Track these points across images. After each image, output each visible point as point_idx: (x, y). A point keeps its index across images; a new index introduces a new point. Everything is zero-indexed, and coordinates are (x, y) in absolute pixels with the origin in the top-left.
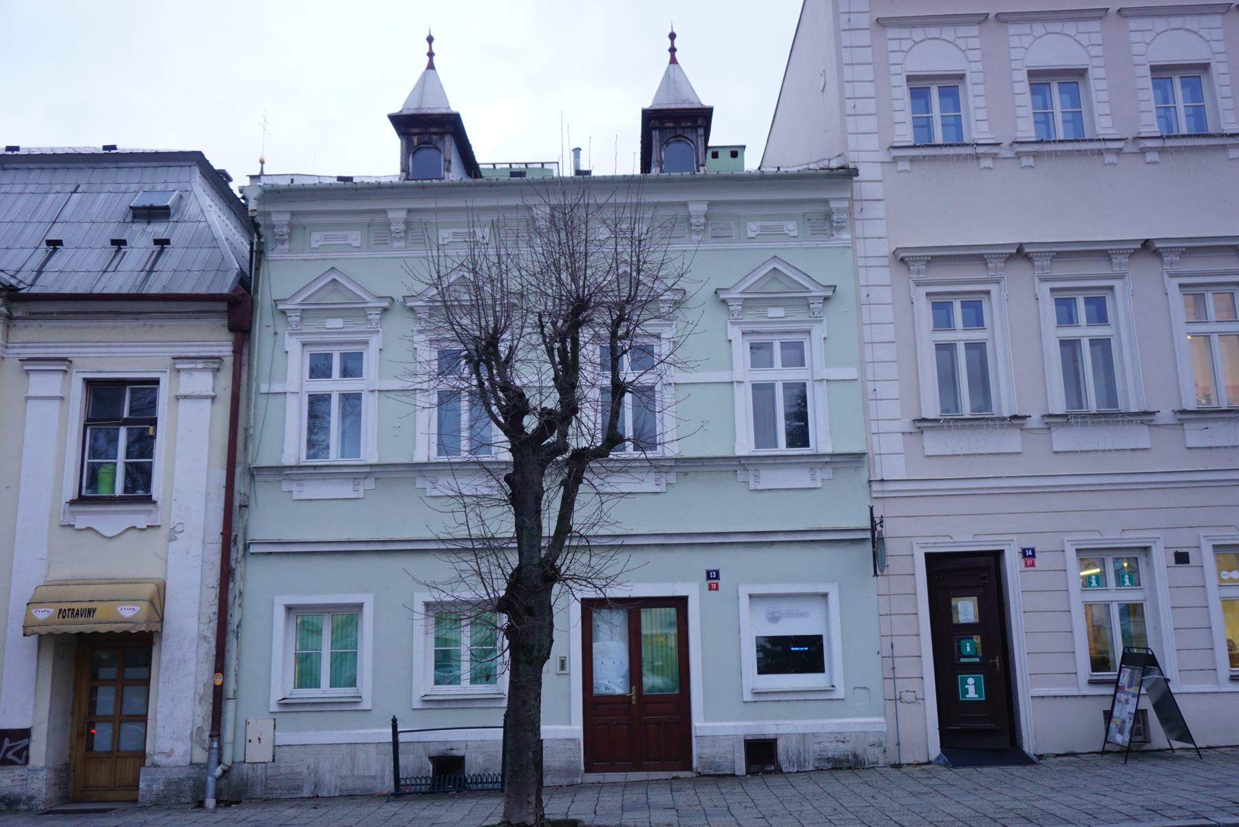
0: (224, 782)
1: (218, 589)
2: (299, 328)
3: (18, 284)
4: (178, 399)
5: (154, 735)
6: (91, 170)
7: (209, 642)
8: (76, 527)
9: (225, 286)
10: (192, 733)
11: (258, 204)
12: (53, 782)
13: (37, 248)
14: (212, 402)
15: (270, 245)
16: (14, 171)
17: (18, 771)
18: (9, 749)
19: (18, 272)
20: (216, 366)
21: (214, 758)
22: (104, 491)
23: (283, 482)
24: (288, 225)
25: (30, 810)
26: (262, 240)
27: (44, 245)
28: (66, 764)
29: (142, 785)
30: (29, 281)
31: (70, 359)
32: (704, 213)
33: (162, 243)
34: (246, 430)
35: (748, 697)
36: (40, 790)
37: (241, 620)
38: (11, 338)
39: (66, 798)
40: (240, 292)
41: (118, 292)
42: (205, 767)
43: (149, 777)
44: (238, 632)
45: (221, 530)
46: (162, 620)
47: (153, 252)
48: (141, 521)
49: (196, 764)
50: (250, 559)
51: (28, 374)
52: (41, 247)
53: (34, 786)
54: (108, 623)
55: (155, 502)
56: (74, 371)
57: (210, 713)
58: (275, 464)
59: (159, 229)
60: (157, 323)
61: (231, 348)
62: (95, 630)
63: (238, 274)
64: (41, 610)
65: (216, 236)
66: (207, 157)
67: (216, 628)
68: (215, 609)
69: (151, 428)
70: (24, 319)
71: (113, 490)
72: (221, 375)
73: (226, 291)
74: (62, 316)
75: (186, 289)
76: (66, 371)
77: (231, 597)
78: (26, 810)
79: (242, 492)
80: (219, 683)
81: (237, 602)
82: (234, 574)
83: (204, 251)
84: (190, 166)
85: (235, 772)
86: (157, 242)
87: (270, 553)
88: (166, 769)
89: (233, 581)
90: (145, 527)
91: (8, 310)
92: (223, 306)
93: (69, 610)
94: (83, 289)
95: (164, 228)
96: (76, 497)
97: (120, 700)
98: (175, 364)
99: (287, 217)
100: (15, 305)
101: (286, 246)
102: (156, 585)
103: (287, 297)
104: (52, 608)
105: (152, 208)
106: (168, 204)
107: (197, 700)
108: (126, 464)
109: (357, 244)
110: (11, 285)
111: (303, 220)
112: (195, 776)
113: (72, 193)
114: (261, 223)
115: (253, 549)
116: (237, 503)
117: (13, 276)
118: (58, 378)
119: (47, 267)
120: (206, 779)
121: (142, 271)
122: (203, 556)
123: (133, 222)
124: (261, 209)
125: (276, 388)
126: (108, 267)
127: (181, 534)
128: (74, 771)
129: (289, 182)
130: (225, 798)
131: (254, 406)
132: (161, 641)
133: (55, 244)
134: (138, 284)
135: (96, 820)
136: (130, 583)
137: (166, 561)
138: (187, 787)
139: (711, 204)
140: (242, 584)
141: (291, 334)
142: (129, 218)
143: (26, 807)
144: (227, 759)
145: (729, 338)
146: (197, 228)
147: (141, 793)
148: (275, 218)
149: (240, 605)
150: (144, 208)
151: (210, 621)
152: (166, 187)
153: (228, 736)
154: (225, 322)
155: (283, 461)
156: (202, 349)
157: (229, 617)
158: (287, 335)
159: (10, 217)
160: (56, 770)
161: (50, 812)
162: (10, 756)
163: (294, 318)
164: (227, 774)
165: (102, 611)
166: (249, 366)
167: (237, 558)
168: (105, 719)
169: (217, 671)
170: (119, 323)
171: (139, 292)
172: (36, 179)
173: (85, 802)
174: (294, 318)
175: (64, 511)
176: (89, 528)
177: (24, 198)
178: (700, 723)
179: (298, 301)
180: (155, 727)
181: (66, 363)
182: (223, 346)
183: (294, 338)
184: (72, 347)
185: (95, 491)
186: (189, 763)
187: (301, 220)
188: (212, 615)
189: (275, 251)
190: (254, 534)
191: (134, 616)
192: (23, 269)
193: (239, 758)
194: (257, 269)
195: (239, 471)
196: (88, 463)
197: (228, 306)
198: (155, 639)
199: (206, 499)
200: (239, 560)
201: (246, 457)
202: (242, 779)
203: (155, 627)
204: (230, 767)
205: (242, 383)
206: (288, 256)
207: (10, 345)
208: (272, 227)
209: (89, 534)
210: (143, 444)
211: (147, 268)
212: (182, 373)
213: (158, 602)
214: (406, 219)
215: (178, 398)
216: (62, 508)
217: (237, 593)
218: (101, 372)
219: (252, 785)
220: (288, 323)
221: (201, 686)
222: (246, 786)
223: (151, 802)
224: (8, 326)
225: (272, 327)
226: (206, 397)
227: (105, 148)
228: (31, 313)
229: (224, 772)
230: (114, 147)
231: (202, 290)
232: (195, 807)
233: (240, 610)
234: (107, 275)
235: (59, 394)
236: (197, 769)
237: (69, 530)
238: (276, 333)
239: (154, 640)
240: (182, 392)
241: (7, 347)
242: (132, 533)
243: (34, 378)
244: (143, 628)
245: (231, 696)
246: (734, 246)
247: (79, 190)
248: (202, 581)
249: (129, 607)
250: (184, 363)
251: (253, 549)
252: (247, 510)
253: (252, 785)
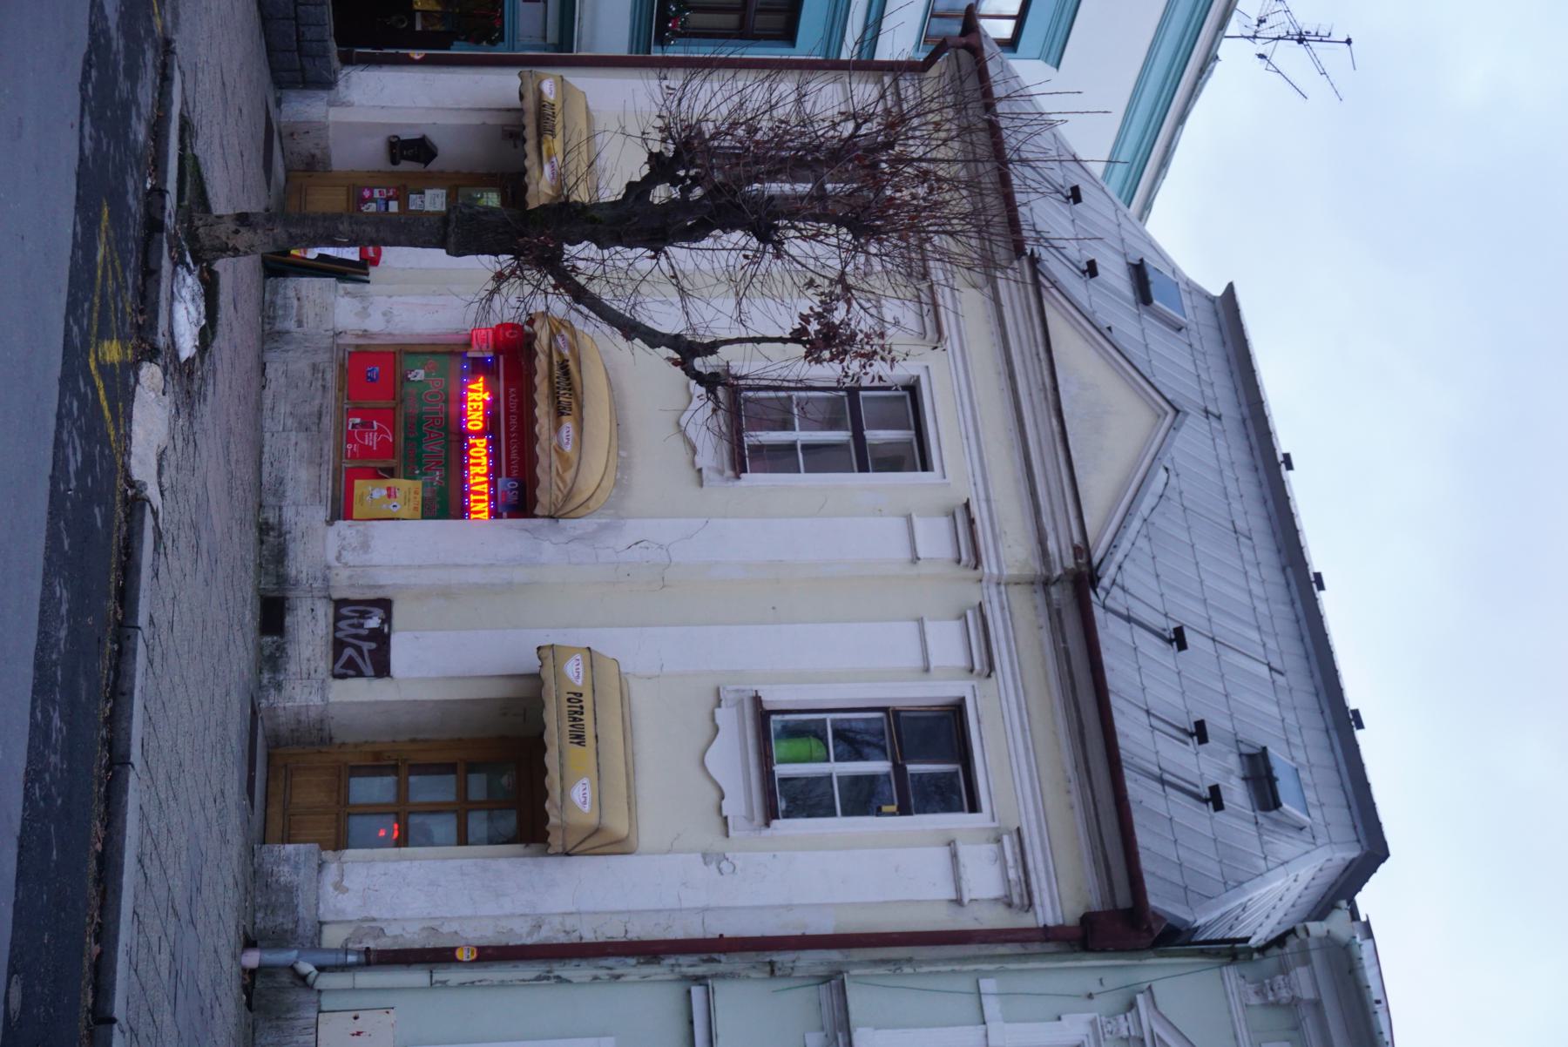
0: (285, 979)
1: (624, 940)
2: (1107, 1036)
3: (1104, 589)
4: (949, 845)
5: (373, 860)
6: (1313, 690)
7: (530, 934)
8: (717, 711)
9: (1159, 899)
10: (374, 920)
11: (1319, 939)
12: (303, 718)
13: (1166, 615)
14: (952, 901)
15: (1248, 970)
16: (1283, 582)
17: (323, 665)
18: (359, 650)
19: (1123, 588)
20: (1016, 900)
21: (329, 959)
22: (778, 748)
23: (823, 1034)
24: (1293, 997)
25: (260, 687)
26: (1256, 956)
27: (1173, 625)
28: (331, 739)
29: (290, 848)
30: (1109, 602)
31: (992, 674)
32: (1299, 995)
33: (1215, 798)
34: (909, 961)
36: (291, 698)
37: (569, 981)
38: (1013, 590)
39: (276, 742)
40: (1154, 926)
41: (1117, 730)
42: (314, 943)
43: (302, 858)
44: (548, 978)
45: (726, 935)
46: (568, 854)
47: (1197, 786)
48: (735, 806)
49: (320, 931)
50: (676, 991)
51: (959, 618)
52: (1169, 621)
53: (298, 690)
54: (562, 765)
55: (767, 825)
56: (975, 683)
57: (408, 946)
58: (853, 1017)
59: (1237, 793)
60: (1075, 798)
61: (1051, 923)
62: (550, 793)
63: (1186, 922)
64: (581, 667)
65: (1245, 885)
66: (1382, 867)
67: (555, 942)
68: (589, 937)
69: (893, 808)
70: (1049, 604)
71: (783, 761)
72: (1001, 910)
73: (1153, 901)
74: (1063, 656)
75: (1142, 838)
76: (972, 670)
77: (611, 962)
78: (260, 682)
79: (797, 964)
80: (461, 955)
81: (602, 973)
82: (652, 963)
83: (1217, 868)
84: (1358, 841)
85: (303, 996)
86: (1215, 790)
87: (691, 1022)
88: (314, 884)
89: (639, 963)
90: (724, 813)
91: (1058, 579)
92: (1123, 899)
93: (582, 707)
94: (1112, 680)
95: (1240, 803)
96: (767, 707)
97: (435, 809)
98: (1010, 833)
99: (1307, 993)
100: (1069, 590)
101: (1255, 1000)
102: (628, 837)
103: (1161, 1007)
104: (583, 682)
105: (1272, 781)
106: (1156, 302)
107: (431, 924)
108: (830, 777)
110: (1099, 579)
111: (1309, 1025)
112: (300, 930)
113: (1268, 665)
114: (1287, 950)
115: (697, 992)
116: (778, 957)
117: (1114, 582)
118: (960, 660)
119: (1137, 629)
120: (295, 948)
121: (1160, 769)
122: (681, 910)
123: (1241, 755)
124: (1312, 944)
125: (992, 1007)
126: (1154, 716)
127: (717, 871)
128: (320, 752)
129: (1376, 997)
130: (257, 983)
131: (953, 971)
132: (532, 856)
133: (1178, 639)
134: (1137, 761)
135: (235, 770)
136: (629, 797)
137: (669, 852)
138: (282, 920)
139: (1317, 1004)
140: (636, 978)
141: (1093, 1023)
142: (1245, 749)
143: (265, 681)
144: (326, 981)
145: (1063, 1017)
146: (1255, 855)
147: (276, 848)
148: (1301, 975)
149: (596, 978)
150: (1269, 769)
151: (567, 933)
152: (1307, 785)
153: (365, 979)
154: (1096, 906)
155: (860, 1030)
156: (1043, 875)
157: (575, 962)
158: (1090, 1016)
159: (1208, 582)
160: (322, 721)
161: (254, 713)
162: (348, 652)
163: (1124, 1026)
164: (300, 983)
165: (580, 757)
166: (1024, 954)
167: (680, 965)
168: (402, 791)
169: (480, 949)
170: (1064, 741)
171: (1124, 764)
172: (1282, 616)
173: (268, 772)
174: (1124, 1026)
175: (743, 691)
176: (716, 730)
177: (1245, 598)
179: (1157, 1029)
180: (385, 860)
181: (986, 670)
183: (1087, 1029)
184: (1013, 674)
185: (778, 737)
186: (322, 919)
187: (1308, 1020)
188: (577, 934)
189: (1241, 982)
190: (726, 994)
191: (573, 802)
192: (1128, 597)
193: (327, 1003)
194: (1202, 953)
195: (835, 955)
197: (1124, 911)
198: (534, 847)
199: (782, 906)
200: (677, 969)
201: (860, 964)
202: (289, 1010)
203: (555, 840)
204: (309, 987)
205: (993, 946)
206: (1238, 1012)
207: (1003, 588)
208: (1284, 970)
209: (708, 730)
211: (1167, 777)
212: (994, 847)
214: (1300, 1000)
215: (951, 844)
216: (748, 687)
217: (617, 972)
218: (979, 722)
219: (278, 1027)
220: (1113, 1015)
221: (455, 926)
222: (278, 1018)
223: (260, 865)
224: (1032, 583)
225: (1102, 989)
226: (958, 889)
227: (1318, 576)
228: (1059, 612)
229: (303, 978)
230: (1321, 587)
231: (1146, 863)
232: (245, 933)
233: (588, 979)
234: (1143, 717)
235: (933, 664)
236: (310, 934)
237: (711, 700)
238: (1090, 996)
239: (533, 845)
241: (999, 584)
242: (714, 795)
243: (955, 627)
244: (553, 820)
245: (436, 977)
247: (1276, 676)
248: (639, 912)
249: (588, 796)
250: (1013, 847)
251: (697, 992)
252: (766, 975)
253: (278, 1027)
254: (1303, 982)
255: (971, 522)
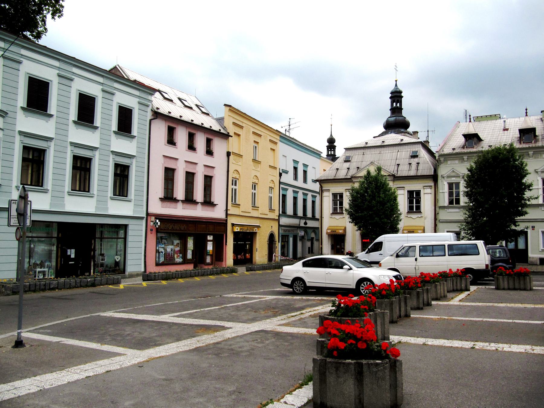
35: (540, 250)
48: (419, 216)
58: (443, 206)
92: (432, 177)
99: (443, 159)
101: (443, 164)
109: (457, 163)
111: (446, 159)
118: (328, 193)
133: (398, 165)
139: (534, 151)
163: (445, 178)
165: (337, 231)
178: (530, 255)
182: (432, 184)
196: (455, 204)
210: (418, 202)
213: (345, 230)
215: (424, 194)
240: (425, 193)
242: (418, 218)
246: (539, 160)
254: (442, 159)
255: (398, 187)
